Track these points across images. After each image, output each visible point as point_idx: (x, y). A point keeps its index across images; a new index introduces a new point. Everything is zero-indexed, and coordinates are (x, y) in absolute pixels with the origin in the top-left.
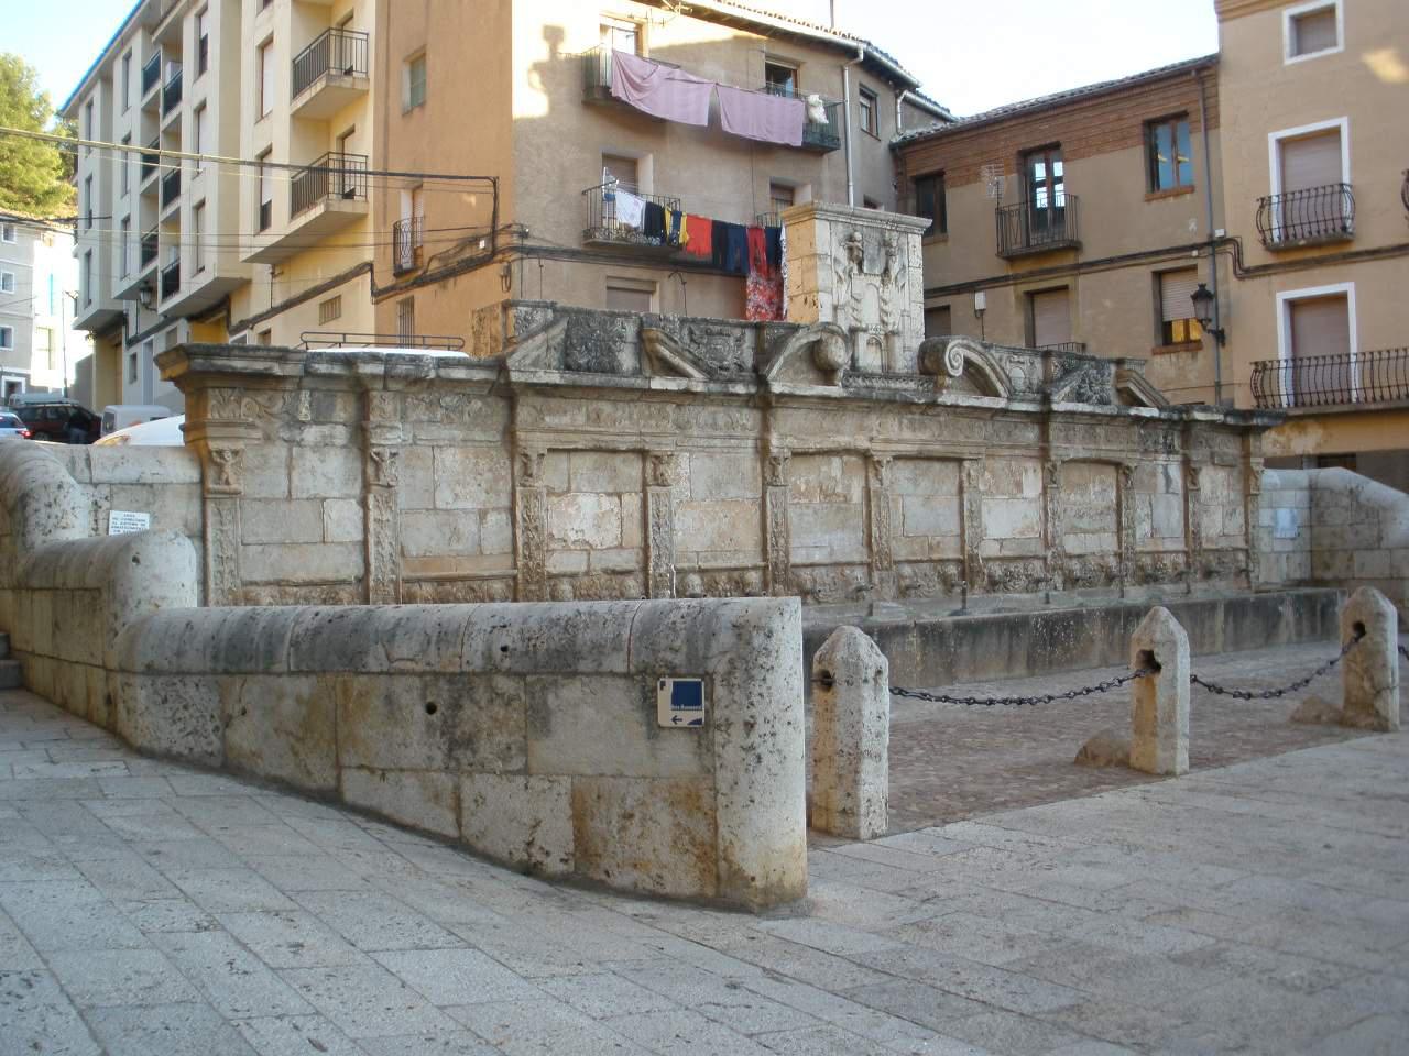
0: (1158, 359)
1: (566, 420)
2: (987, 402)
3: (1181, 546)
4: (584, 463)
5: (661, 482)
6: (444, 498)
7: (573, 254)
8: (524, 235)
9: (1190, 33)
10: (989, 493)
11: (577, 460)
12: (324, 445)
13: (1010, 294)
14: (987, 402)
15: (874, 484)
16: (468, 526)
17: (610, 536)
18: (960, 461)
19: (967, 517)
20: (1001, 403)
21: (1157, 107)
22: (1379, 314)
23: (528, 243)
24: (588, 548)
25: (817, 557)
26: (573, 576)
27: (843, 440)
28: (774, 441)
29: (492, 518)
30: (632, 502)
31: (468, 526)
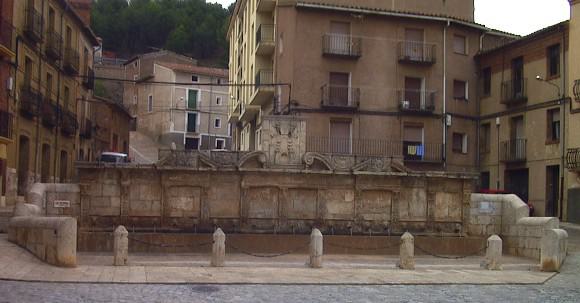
0: (548, 147)
1: (176, 178)
2: (324, 172)
3: (425, 220)
4: (183, 190)
5: (206, 194)
6: (142, 197)
7: (316, 111)
8: (296, 104)
9: (561, 12)
10: (331, 200)
11: (181, 189)
12: (112, 184)
13: (507, 117)
14: (324, 172)
15: (281, 196)
16: (149, 204)
17: (190, 207)
18: (317, 190)
19: (323, 206)
20: (330, 172)
21: (550, 42)
22: (579, 133)
23: (299, 107)
24: (183, 211)
25: (259, 216)
26: (178, 218)
27: (268, 184)
28: (243, 184)
29: (156, 203)
30: (197, 199)
31: (149, 204)
